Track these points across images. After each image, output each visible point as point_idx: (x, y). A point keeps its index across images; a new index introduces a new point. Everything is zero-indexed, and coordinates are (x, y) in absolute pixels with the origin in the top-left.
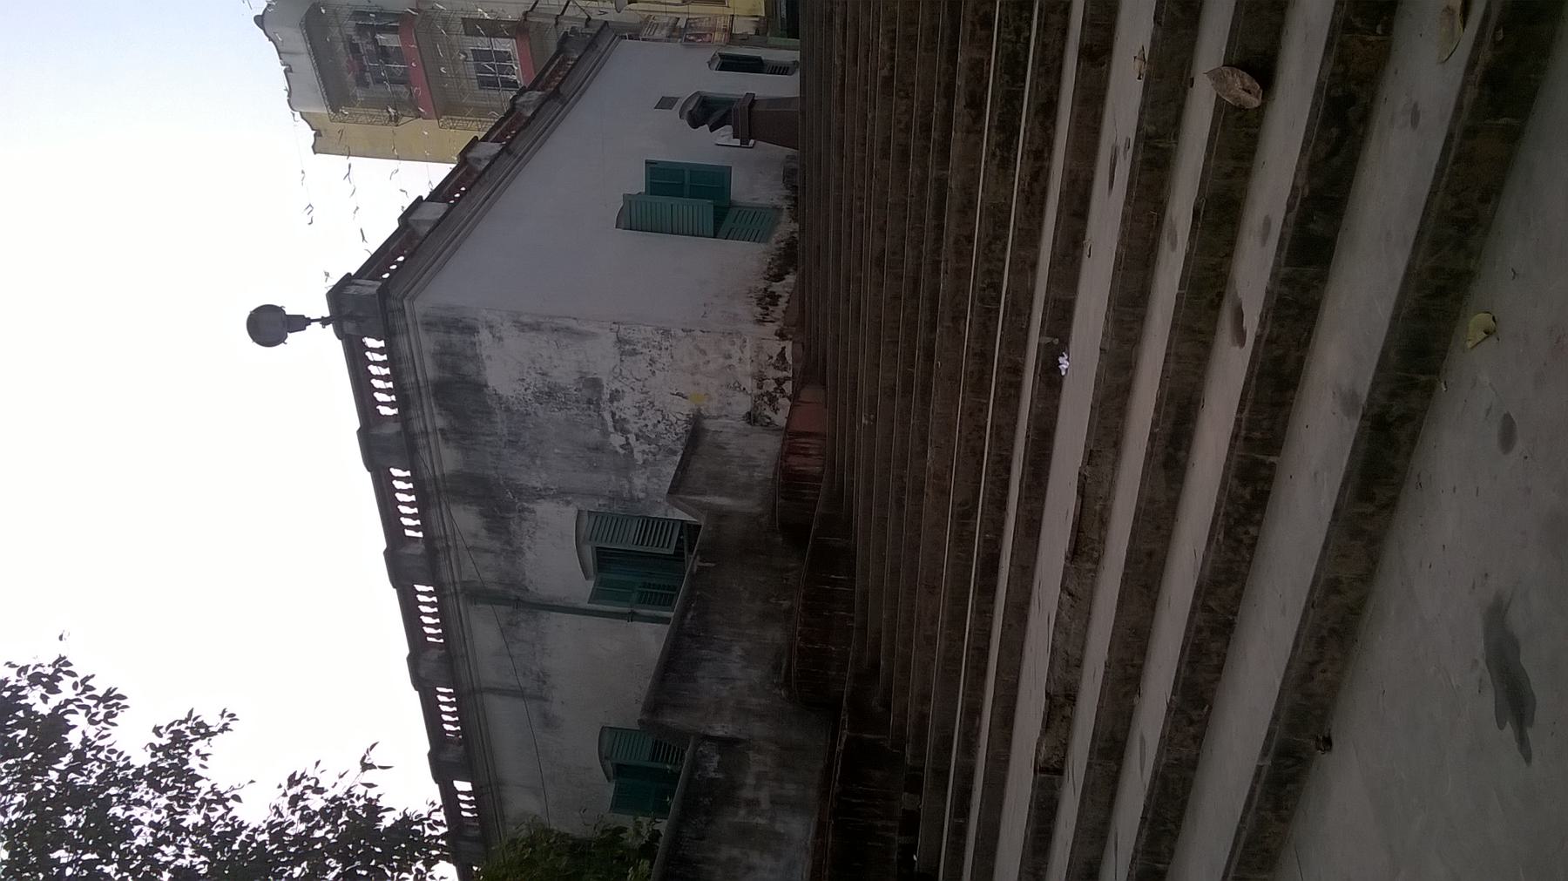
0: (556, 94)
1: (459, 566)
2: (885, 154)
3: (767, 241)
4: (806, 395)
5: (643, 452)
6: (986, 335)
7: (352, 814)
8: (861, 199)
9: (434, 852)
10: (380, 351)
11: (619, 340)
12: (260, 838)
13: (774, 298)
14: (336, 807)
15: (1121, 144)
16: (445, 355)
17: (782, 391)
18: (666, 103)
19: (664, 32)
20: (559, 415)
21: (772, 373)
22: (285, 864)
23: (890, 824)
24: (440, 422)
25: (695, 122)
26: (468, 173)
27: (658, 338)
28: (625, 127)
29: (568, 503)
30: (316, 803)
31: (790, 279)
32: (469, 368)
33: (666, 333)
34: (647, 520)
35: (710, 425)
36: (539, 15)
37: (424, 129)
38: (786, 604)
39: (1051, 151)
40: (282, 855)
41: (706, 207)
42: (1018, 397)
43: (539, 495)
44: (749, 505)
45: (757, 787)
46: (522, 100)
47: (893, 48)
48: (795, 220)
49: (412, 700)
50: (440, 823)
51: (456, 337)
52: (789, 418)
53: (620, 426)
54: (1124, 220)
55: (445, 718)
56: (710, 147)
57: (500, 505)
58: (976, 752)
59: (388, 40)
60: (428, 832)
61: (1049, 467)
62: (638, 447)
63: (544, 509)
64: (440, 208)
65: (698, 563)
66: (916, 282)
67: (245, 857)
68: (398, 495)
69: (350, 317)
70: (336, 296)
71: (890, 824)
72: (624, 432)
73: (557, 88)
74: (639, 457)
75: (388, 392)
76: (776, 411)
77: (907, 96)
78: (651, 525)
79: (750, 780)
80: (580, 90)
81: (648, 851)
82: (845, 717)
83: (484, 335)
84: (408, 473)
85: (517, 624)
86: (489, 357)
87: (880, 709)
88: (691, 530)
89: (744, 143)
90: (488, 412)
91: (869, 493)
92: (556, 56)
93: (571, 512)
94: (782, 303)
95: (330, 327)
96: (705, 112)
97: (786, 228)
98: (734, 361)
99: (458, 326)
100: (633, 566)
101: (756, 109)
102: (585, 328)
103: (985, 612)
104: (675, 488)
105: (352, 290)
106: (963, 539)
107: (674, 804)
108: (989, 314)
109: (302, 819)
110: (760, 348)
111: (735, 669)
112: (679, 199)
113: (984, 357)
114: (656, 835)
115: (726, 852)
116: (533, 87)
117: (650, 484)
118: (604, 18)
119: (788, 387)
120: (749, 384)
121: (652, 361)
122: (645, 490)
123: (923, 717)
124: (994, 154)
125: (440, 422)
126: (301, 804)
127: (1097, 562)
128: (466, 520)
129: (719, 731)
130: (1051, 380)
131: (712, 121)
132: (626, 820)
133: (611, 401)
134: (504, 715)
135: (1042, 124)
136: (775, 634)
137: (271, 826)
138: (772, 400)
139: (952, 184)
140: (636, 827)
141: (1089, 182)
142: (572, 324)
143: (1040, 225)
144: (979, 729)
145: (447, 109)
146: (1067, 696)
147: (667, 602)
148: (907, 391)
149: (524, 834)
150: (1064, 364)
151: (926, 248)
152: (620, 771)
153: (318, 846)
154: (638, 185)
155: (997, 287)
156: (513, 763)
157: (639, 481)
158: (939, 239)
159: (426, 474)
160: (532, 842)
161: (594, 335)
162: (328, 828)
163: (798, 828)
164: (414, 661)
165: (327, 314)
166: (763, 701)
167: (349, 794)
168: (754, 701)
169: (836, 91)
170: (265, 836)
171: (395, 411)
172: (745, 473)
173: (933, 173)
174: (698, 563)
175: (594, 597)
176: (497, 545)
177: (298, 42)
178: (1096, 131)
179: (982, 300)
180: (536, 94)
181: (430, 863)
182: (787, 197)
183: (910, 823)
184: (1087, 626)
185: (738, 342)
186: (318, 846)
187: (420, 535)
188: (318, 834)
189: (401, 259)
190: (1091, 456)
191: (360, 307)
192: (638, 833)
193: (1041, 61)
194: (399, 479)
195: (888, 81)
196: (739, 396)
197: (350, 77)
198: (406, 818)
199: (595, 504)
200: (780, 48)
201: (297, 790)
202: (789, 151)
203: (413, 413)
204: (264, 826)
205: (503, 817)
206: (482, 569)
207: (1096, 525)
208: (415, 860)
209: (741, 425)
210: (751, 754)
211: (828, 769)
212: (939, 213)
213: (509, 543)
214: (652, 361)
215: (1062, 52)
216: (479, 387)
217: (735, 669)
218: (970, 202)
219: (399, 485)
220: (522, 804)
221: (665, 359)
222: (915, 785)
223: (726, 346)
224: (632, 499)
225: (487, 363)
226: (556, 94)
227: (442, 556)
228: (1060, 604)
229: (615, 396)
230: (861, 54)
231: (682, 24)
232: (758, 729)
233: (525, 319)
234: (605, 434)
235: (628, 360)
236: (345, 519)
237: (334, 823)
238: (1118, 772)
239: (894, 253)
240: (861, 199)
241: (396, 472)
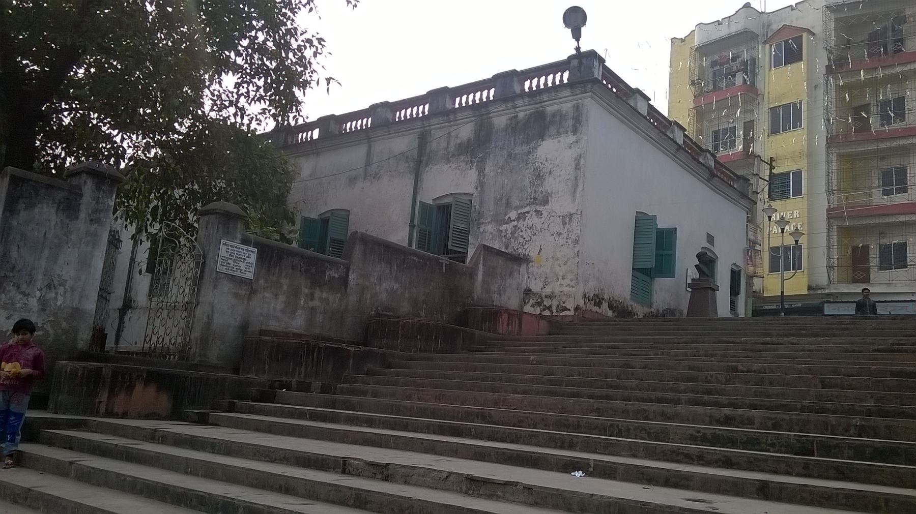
0: (713, 175)
1: (440, 128)
2: (691, 368)
3: (631, 299)
4: (543, 323)
5: (507, 230)
6: (591, 428)
7: (301, 74)
8: (662, 354)
9: (280, 119)
10: (561, 80)
11: (571, 215)
12: (289, 23)
13: (598, 304)
14: (303, 62)
15: (714, 505)
16: (559, 117)
17: (544, 310)
18: (710, 239)
19: (752, 237)
20: (527, 182)
21: (555, 303)
22: (274, 37)
23: (302, 375)
24: (521, 115)
25: (700, 256)
26: (665, 127)
27: (573, 237)
28: (697, 216)
29: (477, 188)
30: (308, 53)
31: (610, 313)
32: (553, 130)
33: (576, 242)
34: (467, 233)
35: (523, 268)
36: (759, 165)
37: (688, 101)
38: (423, 314)
39: (703, 465)
40: (279, 35)
41: (651, 264)
42: (555, 447)
43: (481, 172)
44: (478, 291)
45: (321, 299)
46: (708, 155)
47: (755, 372)
48: (645, 316)
49: (421, 90)
50: (296, 122)
51: (570, 122)
52: (528, 314)
53: (521, 217)
54: (670, 507)
55: (354, 123)
56: (686, 264)
57: (475, 150)
58: (347, 424)
59: (739, 80)
60: (291, 115)
61: (517, 465)
62: (509, 227)
63: (473, 174)
64: (644, 111)
65: (445, 262)
66: (617, 387)
67: (278, 14)
68: (479, 93)
69: (580, 63)
70: (592, 55)
71: (302, 375)
72: (518, 219)
73: (717, 176)
74: (504, 227)
75: (538, 86)
76: (533, 306)
77: (727, 381)
78: (464, 235)
79: (324, 295)
80: (716, 189)
81: (283, 238)
82: (362, 348)
83: (572, 138)
84: (492, 98)
85: (407, 162)
86: (559, 141)
87: (366, 369)
88: (462, 258)
89: (690, 285)
90: (527, 142)
91: (489, 361)
92: (735, 174)
93: (471, 190)
94: (596, 309)
95: (574, 52)
96: (706, 262)
97: (640, 311)
98: (561, 281)
99: (578, 122)
100: (441, 226)
101: (710, 291)
102: (578, 195)
103: (429, 429)
104: (488, 250)
105: (596, 63)
106: (469, 416)
107: (310, 252)
108: (603, 430)
109: (299, 46)
110: (569, 296)
111: (386, 285)
112: (655, 248)
113: (578, 427)
114: (289, 242)
115: (285, 282)
116: (716, 162)
117: (488, 234)
118: (759, 202)
119: (546, 313)
120: (548, 290)
121: (559, 234)
122: (484, 232)
123: (364, 393)
124: (698, 432)
125: (521, 115)
126: (308, 45)
127: (466, 493)
128: (466, 131)
129: (352, 277)
130: (568, 467)
131: (702, 266)
132: (298, 225)
133: (536, 211)
134: (355, 156)
135: (720, 460)
136: (405, 307)
137: (296, 29)
138: (539, 304)
139: (679, 407)
140: (294, 232)
141: (687, 488)
142: (580, 188)
143: (659, 460)
144: (361, 426)
145: (700, 114)
146: (387, 476)
147: (421, 245)
148: (552, 383)
149: (290, 169)
150: (579, 474)
151: (638, 393)
152: (325, 221)
153: (284, 55)
154: (661, 224)
155: (619, 434)
156: (327, 162)
157: (490, 228)
158: (644, 400)
159: (492, 108)
160: (287, 173)
161: (574, 200)
162: (294, 60)
163: (298, 323)
164: (385, 105)
165: (582, 50)
166: (368, 301)
167: (313, 71)
168: (369, 296)
169: (725, 338)
170: (289, 26)
171: (527, 90)
172: (496, 289)
173: (683, 396)
174: (445, 262)
175: (423, 204)
176: (452, 149)
177: (735, 28)
178: (718, 491)
179: (612, 426)
180: (712, 164)
181: (274, 116)
182: (658, 310)
183: (304, 387)
184: (429, 487)
185: (572, 284)
186: (284, 55)
187: (457, 106)
188: (291, 55)
189: (614, 90)
190: (529, 489)
191: (587, 71)
192: (290, 232)
193: (756, 459)
194: (488, 93)
195: (735, 369)
196: (540, 285)
197: (716, 57)
198: (300, 103)
199: (476, 203)
200: (746, 306)
201: (315, 43)
202: (685, 311)
203: (526, 100)
204: (295, 25)
205: (299, 157)
206: (438, 140)
207: (488, 492)
208: (276, 108)
209: (524, 286)
210: (339, 295)
211: (331, 340)
212: (659, 400)
213: (453, 155)
214: (559, 234)
215: (763, 471)
216: (542, 136)
217: (386, 285)
218: (669, 418)
219: (558, 76)
220: (306, 167)
221: (561, 242)
222: (325, 390)
223: (570, 276)
224: (479, 224)
225: (556, 141)
226: (713, 175)
227: (445, 118)
228: (441, 472)
229: (539, 213)
230: (749, 353)
231: (757, 247)
232: (353, 299)
233: (582, 161)
234: (517, 208)
235: (560, 220)
236: (465, 63)
237: (296, 63)
238: (348, 506)
239: (633, 374)
240: (662, 354)
241: (492, 91)
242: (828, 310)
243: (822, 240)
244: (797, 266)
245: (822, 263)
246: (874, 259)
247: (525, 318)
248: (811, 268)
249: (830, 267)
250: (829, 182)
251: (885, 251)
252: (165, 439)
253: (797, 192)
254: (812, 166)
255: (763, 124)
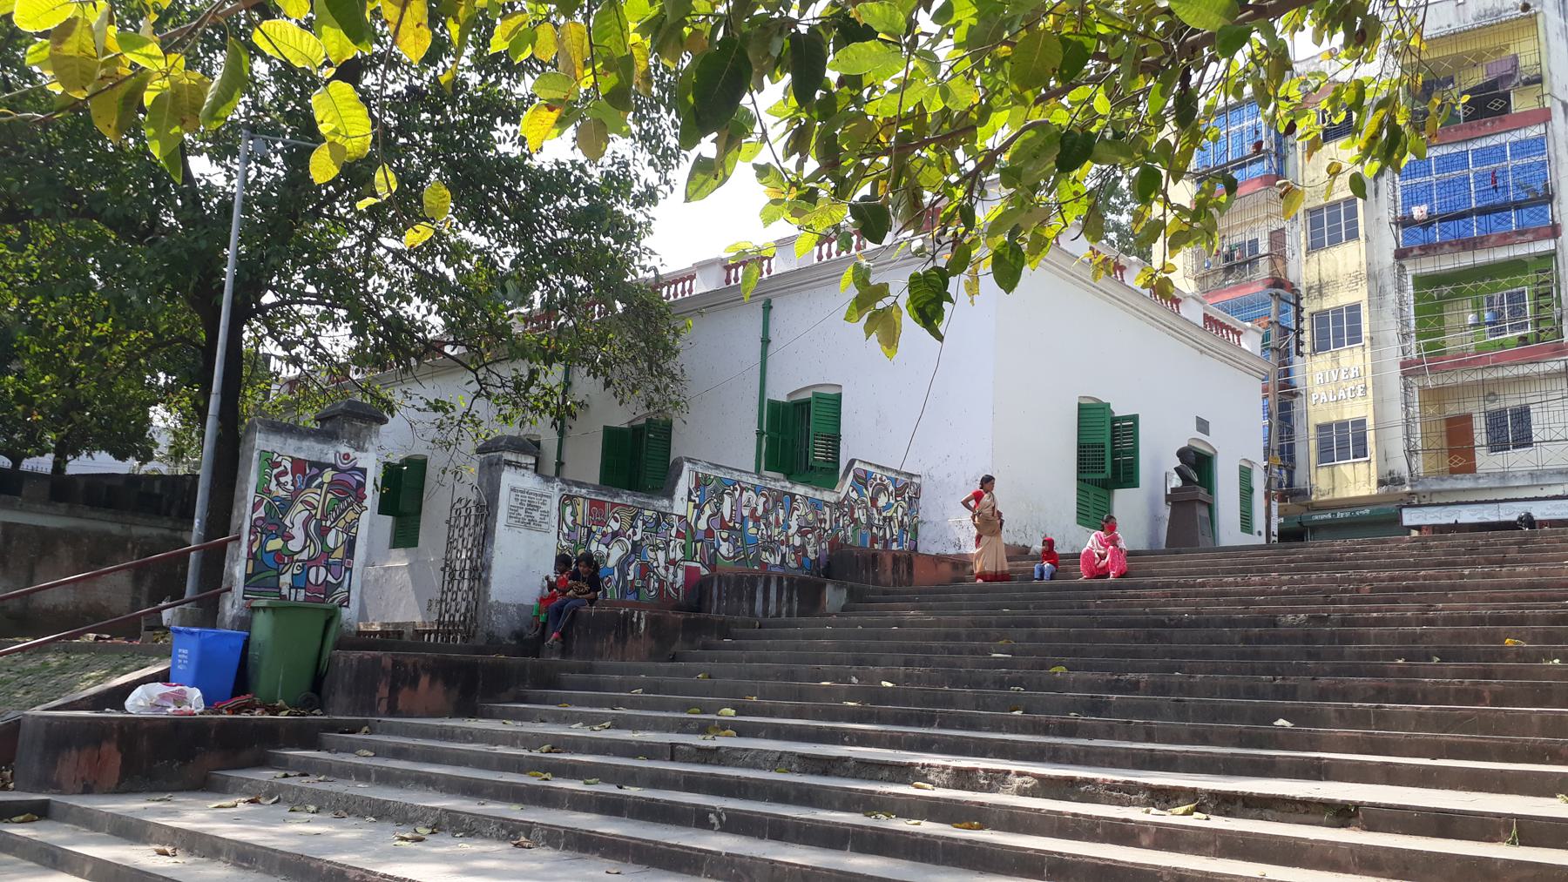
96: (1197, 465)
242: (1410, 517)
243: (1396, 413)
244: (1361, 451)
245: (1398, 447)
246: (1480, 436)
247: (917, 563)
248: (1385, 457)
249: (1410, 452)
250: (1404, 323)
251: (1496, 421)
252: (469, 736)
253: (1355, 337)
254: (1377, 294)
255: (1298, 237)
